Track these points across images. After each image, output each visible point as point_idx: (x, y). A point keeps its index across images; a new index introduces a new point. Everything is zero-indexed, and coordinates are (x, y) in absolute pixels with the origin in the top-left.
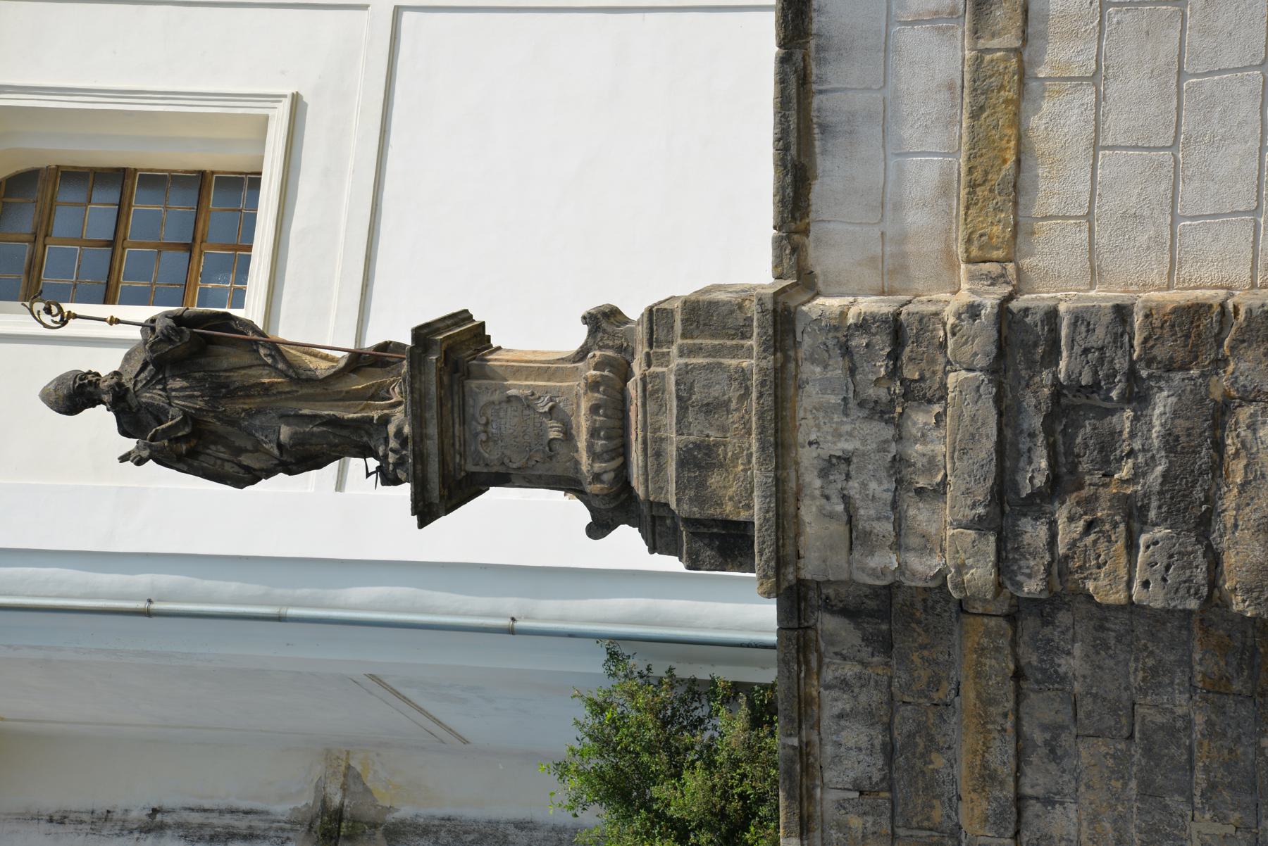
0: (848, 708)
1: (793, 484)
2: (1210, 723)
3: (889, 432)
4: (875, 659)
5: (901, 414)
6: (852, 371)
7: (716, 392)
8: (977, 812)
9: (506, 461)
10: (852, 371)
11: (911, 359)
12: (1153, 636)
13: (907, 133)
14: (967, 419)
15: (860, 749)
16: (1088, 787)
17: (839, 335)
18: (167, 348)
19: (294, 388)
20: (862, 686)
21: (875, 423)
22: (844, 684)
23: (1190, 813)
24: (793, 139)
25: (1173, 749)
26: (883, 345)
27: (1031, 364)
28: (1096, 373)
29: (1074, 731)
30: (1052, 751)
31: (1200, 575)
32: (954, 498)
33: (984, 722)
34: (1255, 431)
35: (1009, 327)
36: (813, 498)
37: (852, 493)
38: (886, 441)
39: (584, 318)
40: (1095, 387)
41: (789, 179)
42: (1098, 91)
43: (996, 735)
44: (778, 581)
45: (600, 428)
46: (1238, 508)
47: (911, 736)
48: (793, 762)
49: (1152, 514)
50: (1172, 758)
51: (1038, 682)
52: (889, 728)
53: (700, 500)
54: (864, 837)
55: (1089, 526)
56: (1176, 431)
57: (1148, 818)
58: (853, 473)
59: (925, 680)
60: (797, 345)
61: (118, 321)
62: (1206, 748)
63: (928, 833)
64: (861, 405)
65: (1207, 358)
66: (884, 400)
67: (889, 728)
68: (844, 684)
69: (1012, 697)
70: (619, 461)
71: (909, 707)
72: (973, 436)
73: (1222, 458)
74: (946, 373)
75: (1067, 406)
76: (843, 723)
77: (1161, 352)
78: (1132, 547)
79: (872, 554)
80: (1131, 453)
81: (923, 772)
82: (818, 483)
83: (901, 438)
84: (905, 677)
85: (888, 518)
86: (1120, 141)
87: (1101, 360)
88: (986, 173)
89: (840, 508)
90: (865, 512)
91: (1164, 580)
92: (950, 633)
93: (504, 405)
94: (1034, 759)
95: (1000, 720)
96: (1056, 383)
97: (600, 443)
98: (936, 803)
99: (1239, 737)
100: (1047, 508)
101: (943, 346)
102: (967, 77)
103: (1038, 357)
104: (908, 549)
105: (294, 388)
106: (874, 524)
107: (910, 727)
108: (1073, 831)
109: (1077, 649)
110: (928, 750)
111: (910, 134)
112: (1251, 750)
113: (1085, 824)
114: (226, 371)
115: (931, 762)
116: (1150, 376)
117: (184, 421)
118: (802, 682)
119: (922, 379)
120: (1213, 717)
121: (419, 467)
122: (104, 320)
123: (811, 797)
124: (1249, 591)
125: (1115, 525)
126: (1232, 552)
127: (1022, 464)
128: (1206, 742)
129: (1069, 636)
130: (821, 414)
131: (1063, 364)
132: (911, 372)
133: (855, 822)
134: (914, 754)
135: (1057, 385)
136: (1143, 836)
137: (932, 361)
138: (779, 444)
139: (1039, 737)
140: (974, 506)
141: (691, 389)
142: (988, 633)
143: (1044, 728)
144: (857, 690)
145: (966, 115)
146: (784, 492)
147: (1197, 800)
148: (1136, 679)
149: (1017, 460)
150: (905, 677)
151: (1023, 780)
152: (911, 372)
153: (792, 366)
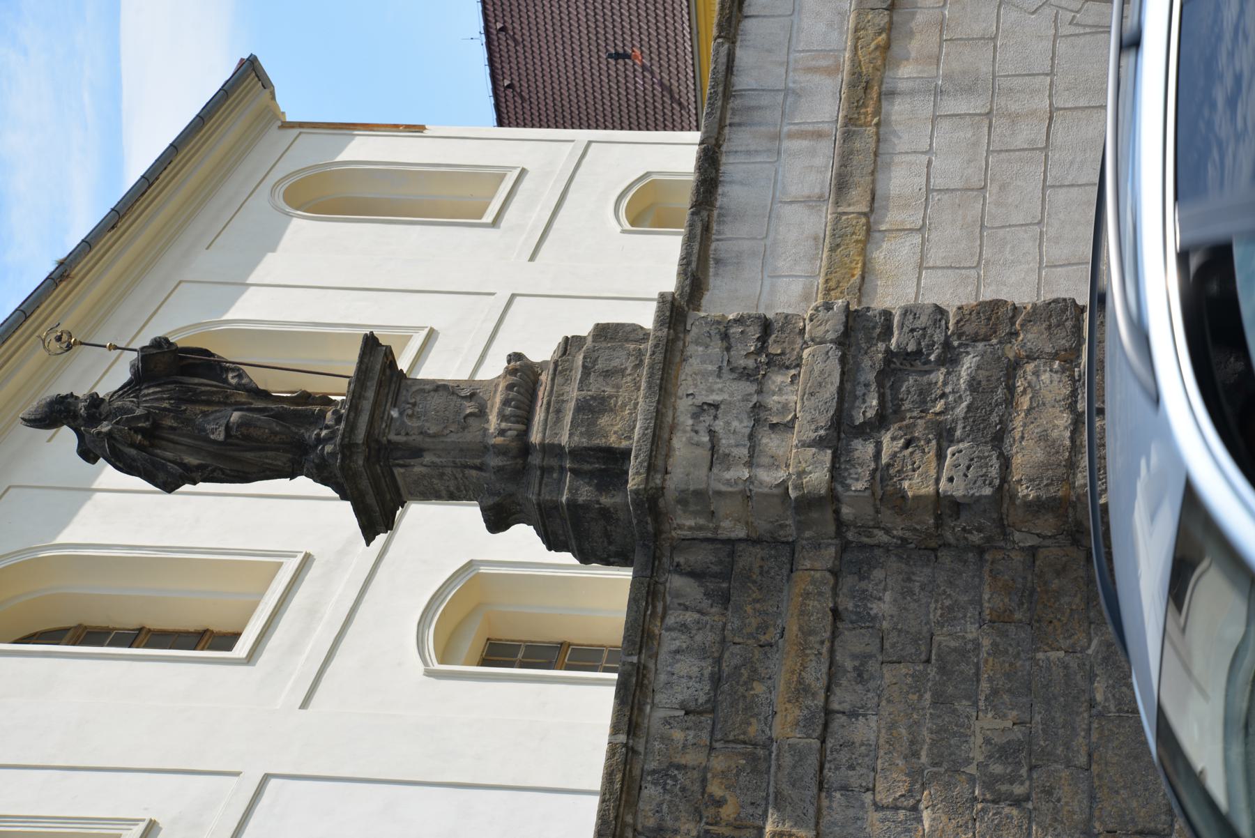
0: (684, 646)
2: (995, 644)
4: (714, 610)
5: (764, 375)
6: (728, 349)
7: (616, 363)
8: (789, 718)
11: (775, 342)
12: (951, 583)
13: (780, 264)
14: (816, 373)
16: (889, 701)
22: (683, 628)
23: (975, 714)
24: (694, 258)
25: (963, 666)
26: (754, 332)
27: (869, 340)
28: (919, 344)
29: (880, 658)
30: (860, 675)
31: (994, 472)
32: (801, 426)
33: (803, 648)
34: (1038, 376)
35: (854, 320)
36: (685, 432)
37: (717, 429)
38: (750, 394)
40: (918, 353)
41: (688, 282)
42: (923, 237)
43: (813, 657)
44: (647, 479)
45: (513, 399)
46: (1025, 425)
48: (630, 675)
49: (958, 433)
50: (962, 672)
51: (852, 622)
52: (718, 661)
53: (589, 434)
54: (684, 746)
55: (907, 445)
56: (979, 378)
57: (939, 721)
59: (754, 625)
60: (687, 332)
62: (990, 662)
64: (732, 370)
65: (1003, 331)
67: (718, 661)
68: (683, 628)
69: (829, 628)
70: (521, 427)
72: (820, 384)
73: (1013, 397)
74: (802, 349)
75: (895, 367)
76: (678, 657)
77: (969, 329)
78: (941, 457)
79: (728, 469)
80: (943, 395)
81: (744, 697)
82: (690, 422)
84: (737, 623)
86: (939, 264)
87: (924, 336)
88: (839, 282)
89: (706, 439)
90: (725, 442)
91: (966, 476)
92: (781, 591)
94: (844, 682)
95: (817, 646)
96: (888, 351)
97: (509, 410)
99: (1018, 654)
100: (875, 434)
101: (802, 331)
102: (828, 228)
103: (875, 335)
104: (758, 466)
107: (736, 661)
108: (873, 737)
109: (888, 596)
111: (783, 265)
112: (1027, 663)
113: (883, 731)
115: (752, 689)
116: (960, 345)
117: (146, 417)
118: (648, 618)
119: (783, 353)
120: (998, 639)
121: (352, 414)
123: (641, 710)
124: (1031, 480)
125: (928, 441)
126: (1019, 456)
127: (857, 404)
128: (991, 659)
129: (881, 587)
130: (699, 377)
131: (894, 341)
132: (775, 349)
133: (678, 735)
134: (738, 683)
135: (888, 351)
136: (934, 736)
137: (793, 342)
138: (664, 388)
139: (849, 665)
140: (816, 430)
141: (595, 361)
142: (813, 582)
143: (854, 657)
145: (826, 250)
147: (981, 703)
148: (935, 616)
149: (854, 402)
150: (737, 623)
151: (832, 698)
152: (775, 349)
153: (681, 344)
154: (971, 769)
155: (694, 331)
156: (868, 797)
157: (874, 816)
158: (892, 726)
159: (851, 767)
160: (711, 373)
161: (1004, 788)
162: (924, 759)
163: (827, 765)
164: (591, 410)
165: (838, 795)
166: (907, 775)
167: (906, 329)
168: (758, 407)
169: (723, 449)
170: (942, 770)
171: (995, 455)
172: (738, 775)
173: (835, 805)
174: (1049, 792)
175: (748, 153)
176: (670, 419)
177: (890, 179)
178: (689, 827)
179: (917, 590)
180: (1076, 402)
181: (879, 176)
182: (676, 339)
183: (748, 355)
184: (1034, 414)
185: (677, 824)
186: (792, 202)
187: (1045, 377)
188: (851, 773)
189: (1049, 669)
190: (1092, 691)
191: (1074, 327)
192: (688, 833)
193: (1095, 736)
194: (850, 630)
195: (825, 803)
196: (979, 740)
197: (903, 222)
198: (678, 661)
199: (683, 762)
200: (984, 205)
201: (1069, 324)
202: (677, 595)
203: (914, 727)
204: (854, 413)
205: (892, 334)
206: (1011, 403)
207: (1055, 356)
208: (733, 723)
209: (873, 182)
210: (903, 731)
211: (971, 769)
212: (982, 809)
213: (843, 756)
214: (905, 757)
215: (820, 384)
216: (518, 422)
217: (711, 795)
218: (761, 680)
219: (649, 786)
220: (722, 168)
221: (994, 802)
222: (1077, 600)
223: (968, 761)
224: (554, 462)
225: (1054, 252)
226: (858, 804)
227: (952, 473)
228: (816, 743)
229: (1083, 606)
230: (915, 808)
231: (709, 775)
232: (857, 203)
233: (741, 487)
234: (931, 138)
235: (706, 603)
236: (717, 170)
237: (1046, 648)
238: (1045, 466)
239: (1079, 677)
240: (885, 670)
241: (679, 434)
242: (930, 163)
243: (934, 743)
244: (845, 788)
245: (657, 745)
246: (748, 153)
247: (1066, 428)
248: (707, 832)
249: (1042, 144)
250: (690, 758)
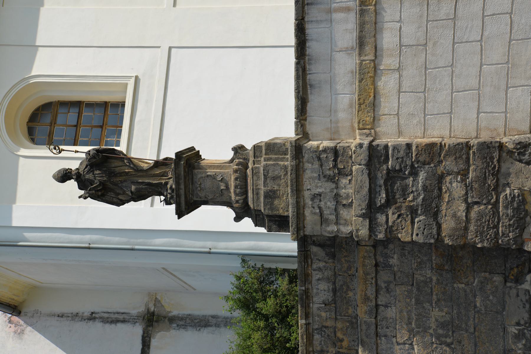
0: (321, 277)
2: (438, 280)
3: (334, 186)
5: (337, 180)
6: (321, 166)
7: (276, 173)
8: (363, 310)
10: (321, 166)
11: (341, 162)
14: (359, 181)
15: (325, 291)
16: (399, 301)
22: (320, 269)
24: (301, 89)
27: (379, 163)
29: (395, 283)
30: (387, 290)
31: (435, 231)
32: (355, 207)
34: (451, 184)
35: (373, 151)
36: (309, 208)
37: (322, 206)
38: (333, 189)
40: (400, 170)
41: (300, 103)
42: (400, 74)
43: (369, 285)
45: (238, 185)
46: (446, 209)
47: (342, 286)
48: (303, 295)
49: (419, 212)
51: (383, 267)
52: (334, 283)
53: (272, 209)
54: (326, 319)
57: (418, 311)
58: (322, 199)
59: (346, 267)
60: (303, 157)
61: (78, 152)
64: (324, 177)
67: (334, 283)
68: (320, 269)
69: (374, 272)
72: (361, 187)
74: (352, 166)
75: (392, 176)
76: (319, 282)
77: (421, 159)
78: (413, 223)
79: (328, 226)
80: (412, 192)
82: (310, 203)
84: (339, 266)
85: (333, 214)
87: (402, 161)
88: (364, 100)
89: (318, 211)
91: (423, 233)
92: (354, 252)
94: (382, 292)
98: (350, 307)
100: (386, 210)
102: (357, 69)
104: (340, 224)
106: (329, 216)
107: (341, 283)
108: (394, 315)
109: (395, 256)
111: (339, 87)
112: (451, 288)
116: (418, 167)
117: (100, 185)
119: (344, 168)
123: (309, 306)
124: (450, 236)
125: (407, 216)
126: (445, 224)
127: (377, 196)
128: (436, 286)
129: (393, 252)
131: (390, 163)
132: (341, 166)
133: (323, 314)
137: (348, 162)
138: (298, 190)
139: (383, 285)
140: (362, 210)
141: (268, 172)
142: (366, 251)
143: (385, 282)
145: (357, 81)
147: (434, 304)
148: (414, 266)
150: (339, 266)
151: (378, 300)
152: (341, 166)
154: (431, 331)
155: (306, 156)
156: (394, 340)
157: (397, 347)
158: (401, 312)
159: (387, 328)
160: (316, 177)
161: (443, 339)
162: (413, 326)
163: (378, 327)
164: (271, 197)
165: (383, 338)
166: (408, 331)
167: (395, 158)
169: (325, 216)
170: (420, 330)
171: (435, 223)
172: (347, 329)
173: (383, 342)
174: (460, 342)
175: (317, 21)
176: (302, 203)
177: (383, 38)
178: (332, 349)
179: (407, 254)
180: (468, 197)
181: (378, 36)
183: (330, 169)
184: (450, 204)
185: (328, 349)
186: (340, 51)
187: (454, 185)
188: (387, 330)
189: (459, 292)
190: (475, 302)
191: (466, 158)
192: (332, 352)
193: (476, 321)
194: (381, 270)
195: (379, 341)
196: (434, 320)
197: (390, 64)
198: (320, 284)
199: (327, 325)
200: (426, 55)
201: (464, 157)
203: (409, 312)
204: (376, 200)
205: (389, 159)
206: (441, 196)
207: (458, 173)
209: (375, 41)
210: (405, 314)
211: (431, 331)
212: (436, 347)
213: (384, 323)
214: (407, 324)
215: (361, 187)
216: (242, 195)
217: (338, 338)
218: (351, 290)
220: (307, 31)
221: (440, 344)
222: (469, 262)
223: (430, 328)
225: (459, 83)
226: (391, 342)
227: (418, 232)
228: (373, 320)
229: (471, 265)
230: (411, 344)
231: (337, 330)
232: (369, 49)
234: (401, 12)
235: (326, 259)
236: (305, 36)
237: (457, 282)
238: (455, 229)
239: (470, 296)
240: (397, 288)
242: (400, 28)
243: (417, 320)
244: (386, 336)
246: (317, 21)
247: (464, 211)
248: (339, 352)
249: (452, 17)
250: (329, 323)
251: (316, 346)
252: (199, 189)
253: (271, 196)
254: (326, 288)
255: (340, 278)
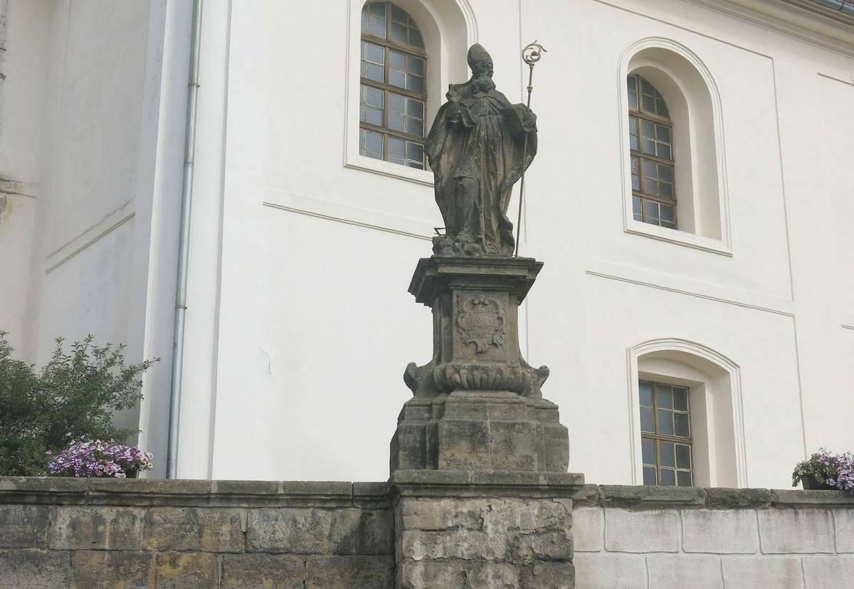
0: (300, 526)
1: (465, 494)
3: (500, 556)
9: (462, 315)
10: (537, 533)
15: (274, 533)
17: (558, 525)
18: (521, 117)
19: (493, 189)
20: (315, 536)
21: (504, 546)
22: (316, 523)
26: (556, 551)
36: (456, 507)
37: (460, 532)
38: (494, 554)
39: (546, 367)
47: (284, 567)
52: (288, 552)
53: (451, 435)
58: (472, 533)
60: (551, 499)
61: (530, 92)
63: (220, 576)
66: (520, 552)
67: (288, 552)
68: (316, 523)
71: (302, 565)
76: (290, 522)
81: (261, 572)
82: (465, 510)
83: (496, 563)
84: (322, 563)
85: (445, 554)
89: (450, 524)
90: (448, 540)
93: (496, 315)
98: (240, 582)
105: (493, 189)
106: (441, 546)
107: (290, 566)
110: (274, 577)
114: (503, 149)
115: (267, 579)
117: (472, 123)
118: (319, 497)
121: (462, 261)
122: (530, 84)
132: (538, 569)
133: (226, 529)
134: (271, 568)
144: (312, 532)
146: (460, 489)
152: (538, 569)
164: (472, 435)
168: (483, 561)
169: (440, 539)
172: (196, 574)
182: (543, 492)
202: (343, 517)
208: (238, 568)
216: (468, 382)
217: (179, 557)
219: (185, 513)
220: (752, 511)
224: (435, 413)
231: (195, 554)
233: (407, 555)
235: (337, 538)
236: (748, 507)
241: (453, 503)
245: (216, 515)
250: (207, 538)
251: (161, 513)
252: (476, 302)
253: (476, 436)
254: (279, 535)
255: (299, 561)
